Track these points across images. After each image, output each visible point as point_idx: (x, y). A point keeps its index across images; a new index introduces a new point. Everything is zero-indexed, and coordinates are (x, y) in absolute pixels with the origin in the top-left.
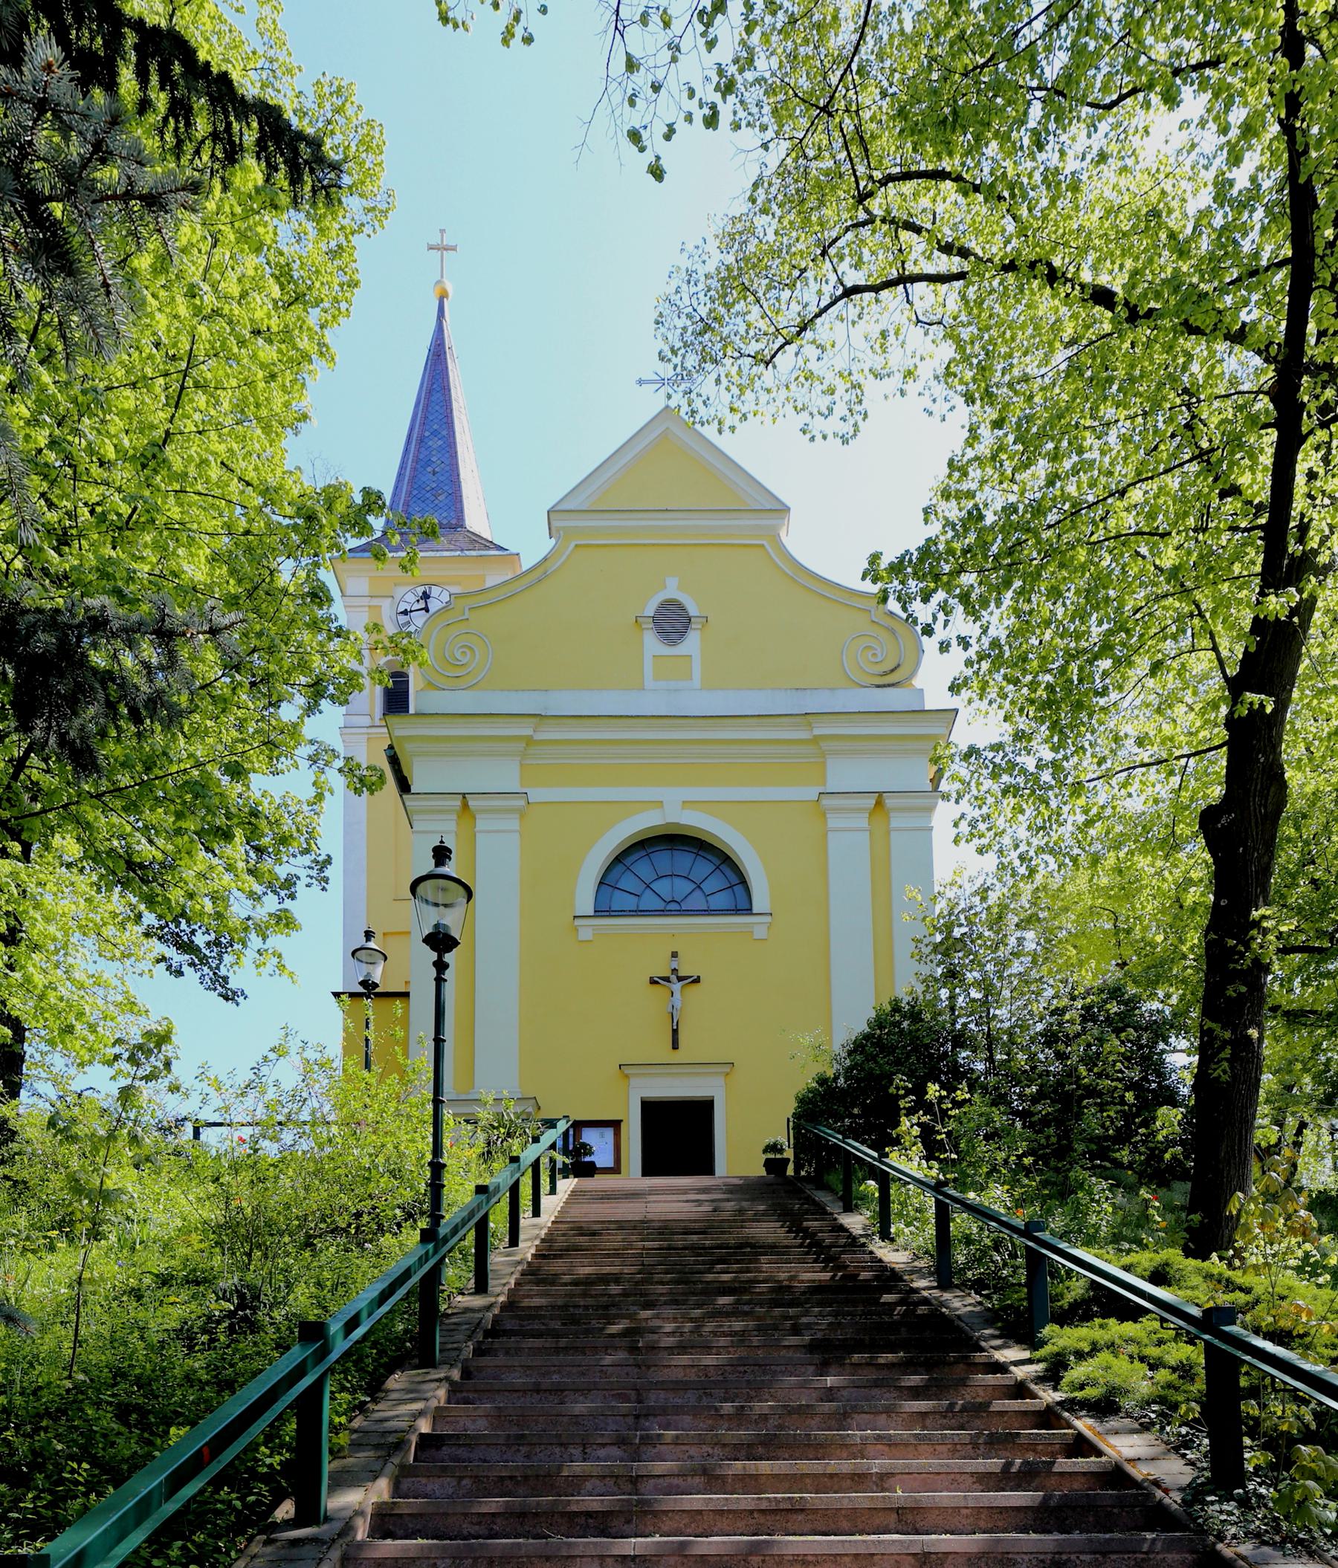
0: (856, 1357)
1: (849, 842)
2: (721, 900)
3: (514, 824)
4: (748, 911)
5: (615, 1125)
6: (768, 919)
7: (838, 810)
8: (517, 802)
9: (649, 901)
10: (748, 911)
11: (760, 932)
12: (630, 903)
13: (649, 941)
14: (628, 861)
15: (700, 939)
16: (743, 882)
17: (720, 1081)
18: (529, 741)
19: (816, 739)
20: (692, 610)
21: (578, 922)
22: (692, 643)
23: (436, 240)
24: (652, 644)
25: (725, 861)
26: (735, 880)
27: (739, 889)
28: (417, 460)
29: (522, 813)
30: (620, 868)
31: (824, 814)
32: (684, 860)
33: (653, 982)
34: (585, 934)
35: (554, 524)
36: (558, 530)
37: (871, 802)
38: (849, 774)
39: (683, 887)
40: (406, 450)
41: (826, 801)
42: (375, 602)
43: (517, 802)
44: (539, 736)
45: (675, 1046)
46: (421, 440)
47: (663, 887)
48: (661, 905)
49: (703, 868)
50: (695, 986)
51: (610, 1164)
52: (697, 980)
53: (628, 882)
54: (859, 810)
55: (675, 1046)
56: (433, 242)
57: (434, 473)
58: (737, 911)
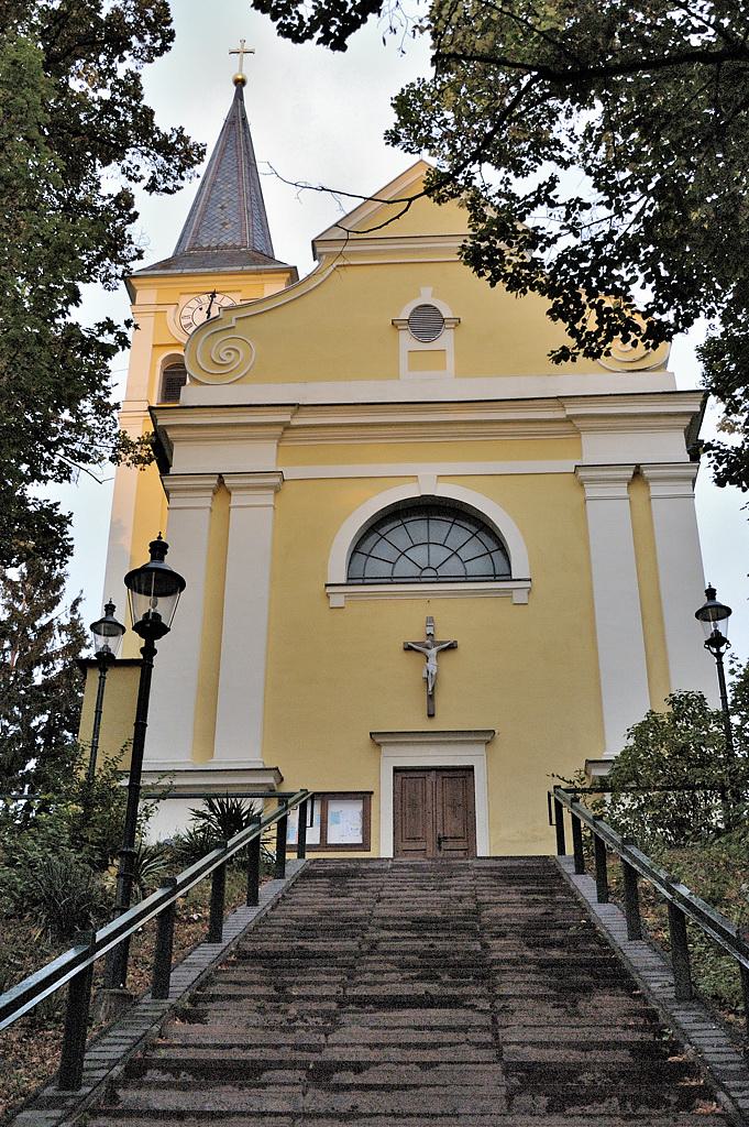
0: (571, 1110)
1: (610, 511)
2: (480, 567)
3: (267, 498)
4: (508, 577)
5: (365, 797)
6: (528, 584)
7: (591, 480)
8: (276, 484)
9: (405, 567)
10: (508, 577)
11: (519, 597)
12: (385, 570)
13: (405, 612)
14: (365, 548)
15: (456, 612)
16: (502, 547)
17: (481, 749)
18: (287, 427)
19: (569, 419)
20: (446, 314)
21: (329, 590)
22: (446, 339)
23: (237, 47)
24: (407, 340)
25: (480, 524)
26: (492, 546)
27: (497, 556)
28: (209, 199)
29: (277, 490)
30: (375, 537)
31: (582, 485)
32: (440, 528)
33: (409, 648)
34: (337, 601)
35: (319, 250)
36: (321, 255)
37: (630, 473)
38: (601, 448)
39: (439, 554)
40: (217, 146)
41: (581, 473)
42: (161, 308)
43: (276, 484)
44: (295, 422)
45: (431, 716)
46: (213, 184)
47: (419, 555)
48: (417, 572)
49: (459, 535)
50: (450, 655)
51: (359, 840)
52: (452, 647)
53: (383, 550)
54: (677, 427)
55: (431, 716)
56: (235, 49)
57: (222, 208)
58: (495, 577)
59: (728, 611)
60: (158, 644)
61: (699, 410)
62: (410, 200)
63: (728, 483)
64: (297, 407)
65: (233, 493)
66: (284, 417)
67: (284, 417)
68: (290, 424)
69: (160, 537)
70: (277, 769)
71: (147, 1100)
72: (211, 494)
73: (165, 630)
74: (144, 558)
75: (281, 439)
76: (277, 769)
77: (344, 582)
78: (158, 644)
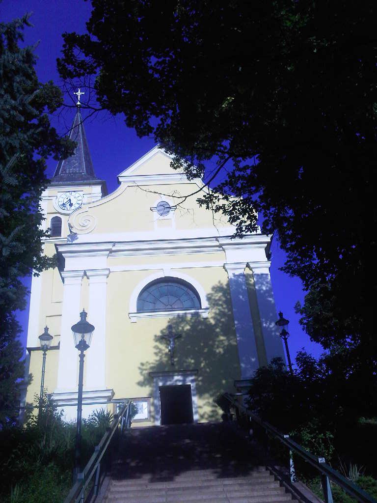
18: (111, 251)
24: (156, 214)
59: (288, 322)
60: (85, 352)
61: (270, 240)
62: (186, 197)
63: (320, 343)
64: (114, 243)
65: (90, 278)
66: (110, 246)
67: (110, 246)
68: (112, 249)
69: (84, 310)
70: (112, 390)
71: (249, 481)
72: (81, 278)
73: (88, 347)
74: (78, 319)
75: (108, 256)
76: (112, 390)
77: (136, 312)
78: (85, 352)
